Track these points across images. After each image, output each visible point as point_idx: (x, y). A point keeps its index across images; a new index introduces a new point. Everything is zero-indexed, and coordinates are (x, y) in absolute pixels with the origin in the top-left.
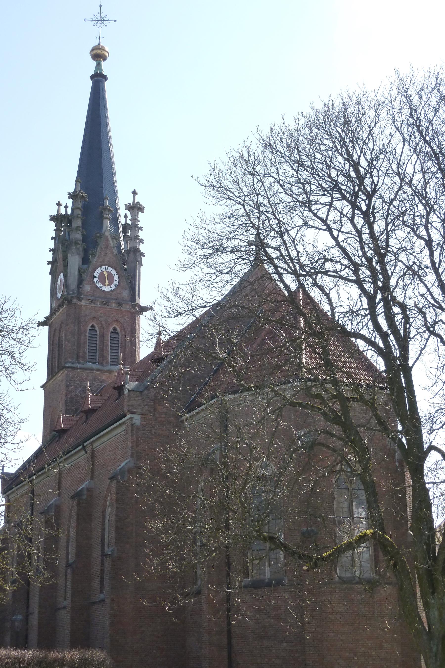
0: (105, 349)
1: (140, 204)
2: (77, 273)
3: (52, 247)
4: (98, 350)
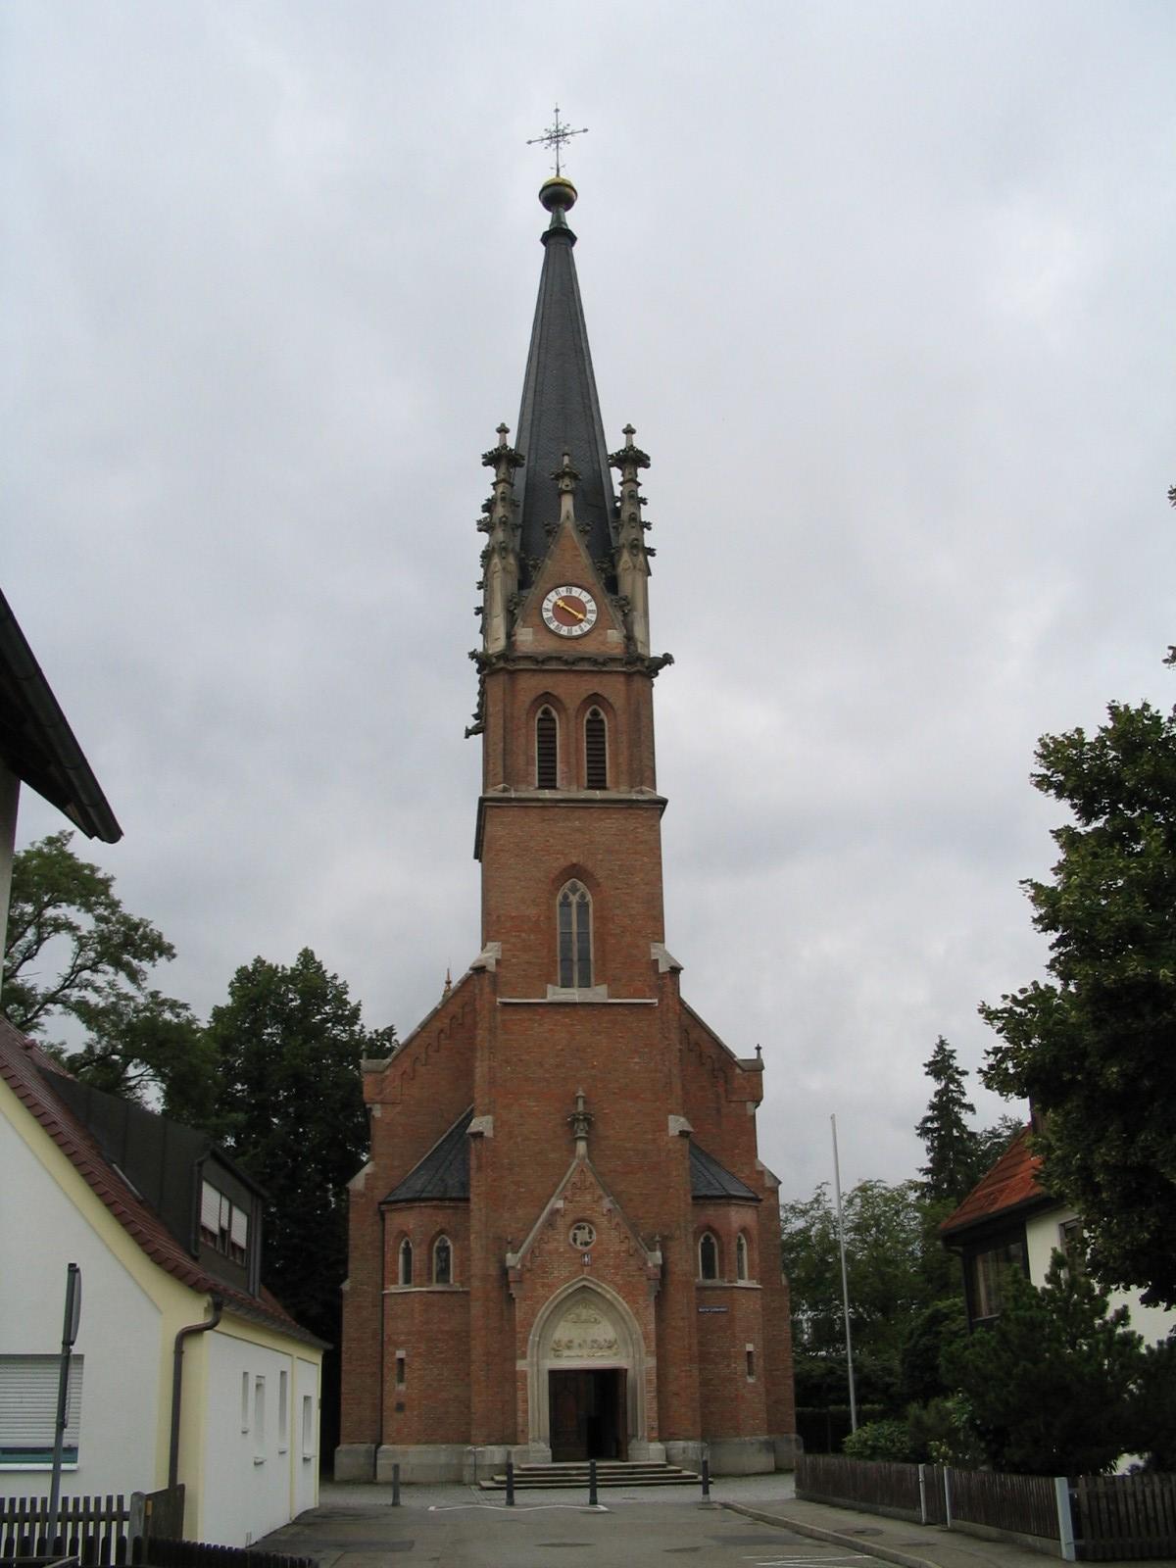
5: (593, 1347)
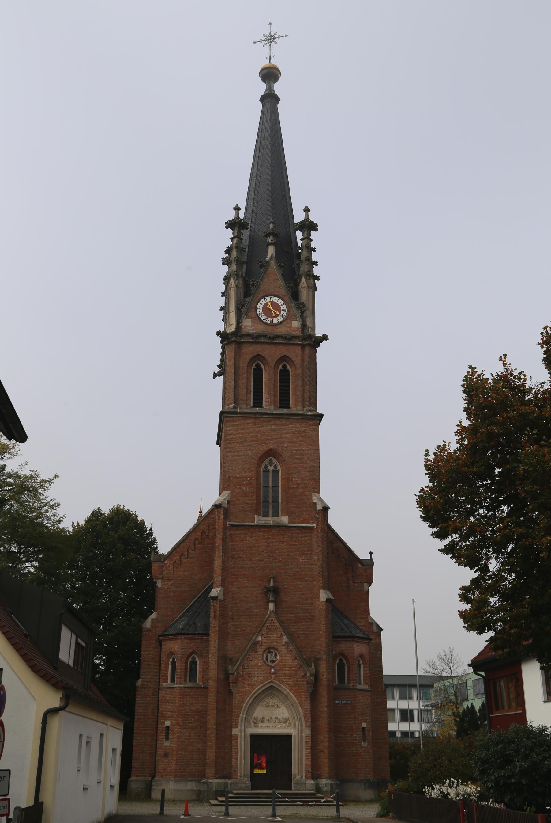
5: (276, 722)
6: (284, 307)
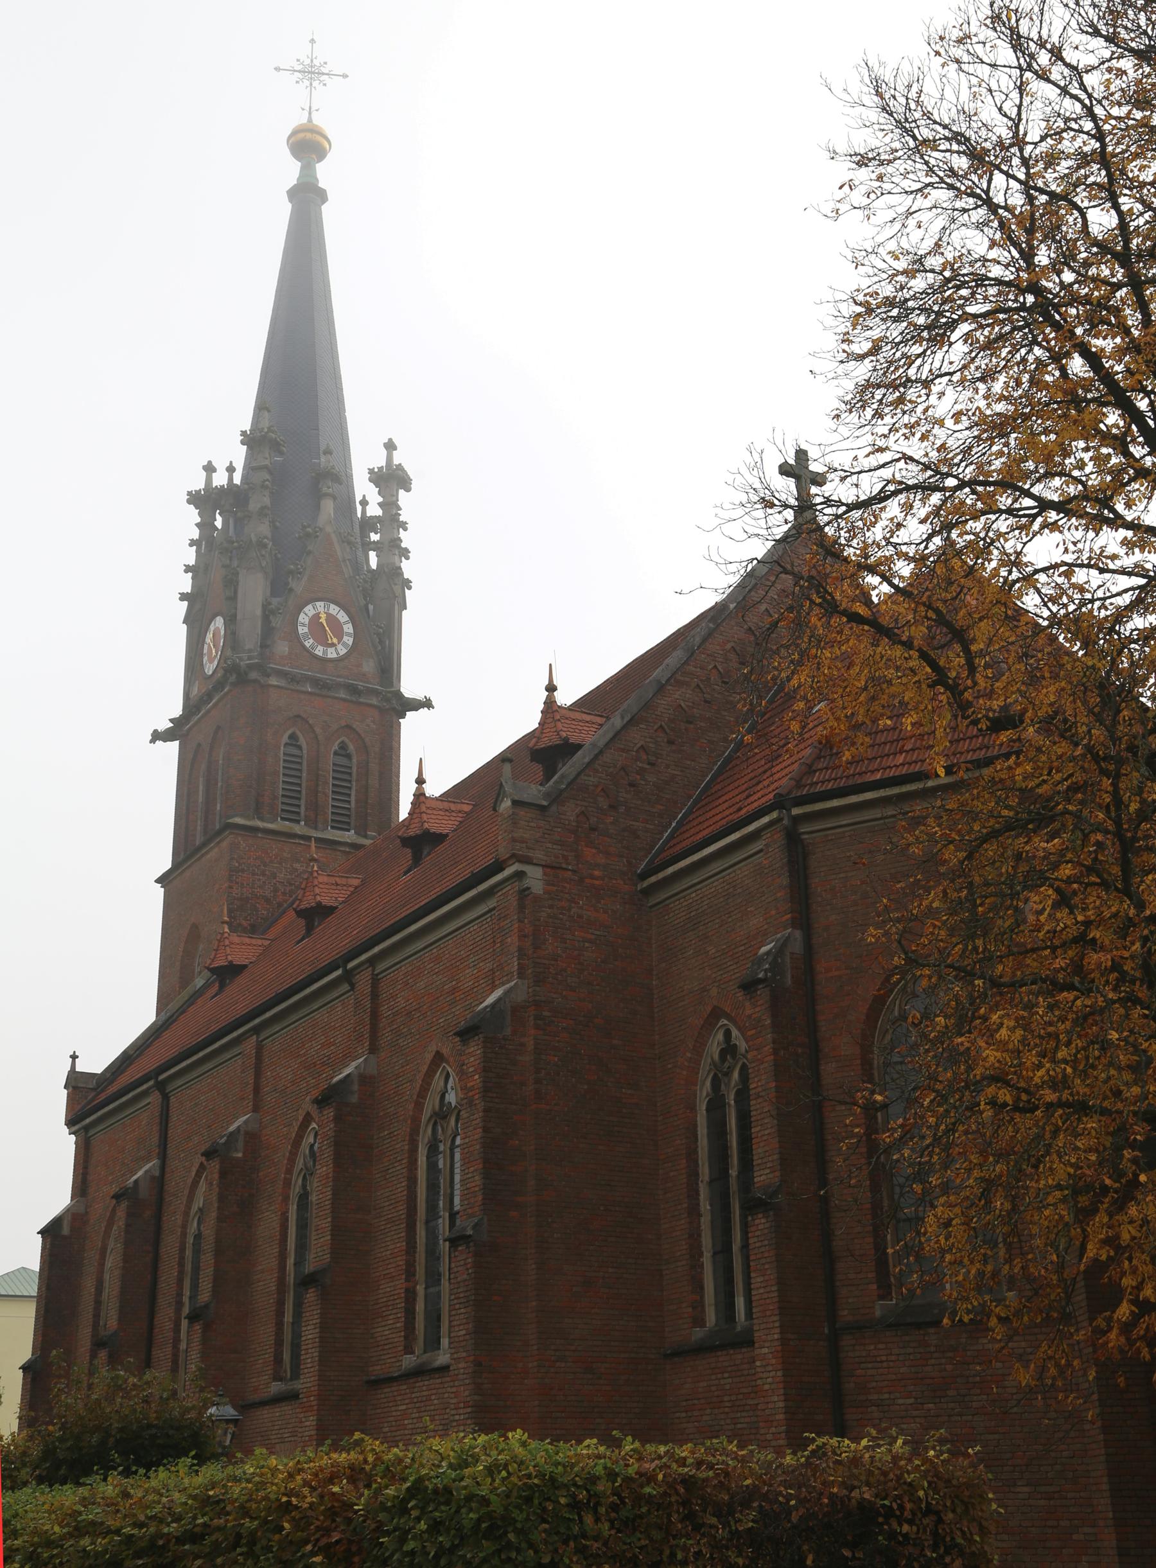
0: (320, 789)
1: (403, 470)
2: (259, 612)
3: (192, 561)
4: (304, 792)
6: (348, 628)
